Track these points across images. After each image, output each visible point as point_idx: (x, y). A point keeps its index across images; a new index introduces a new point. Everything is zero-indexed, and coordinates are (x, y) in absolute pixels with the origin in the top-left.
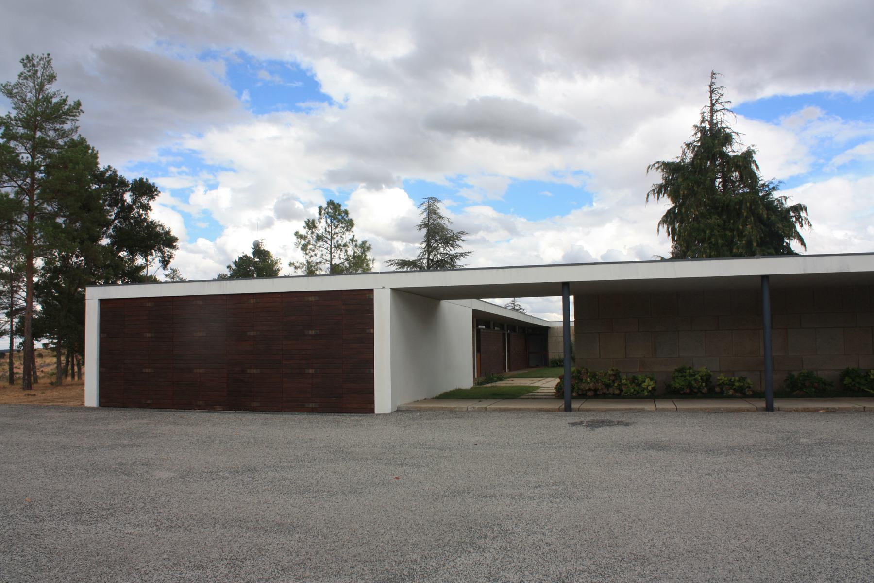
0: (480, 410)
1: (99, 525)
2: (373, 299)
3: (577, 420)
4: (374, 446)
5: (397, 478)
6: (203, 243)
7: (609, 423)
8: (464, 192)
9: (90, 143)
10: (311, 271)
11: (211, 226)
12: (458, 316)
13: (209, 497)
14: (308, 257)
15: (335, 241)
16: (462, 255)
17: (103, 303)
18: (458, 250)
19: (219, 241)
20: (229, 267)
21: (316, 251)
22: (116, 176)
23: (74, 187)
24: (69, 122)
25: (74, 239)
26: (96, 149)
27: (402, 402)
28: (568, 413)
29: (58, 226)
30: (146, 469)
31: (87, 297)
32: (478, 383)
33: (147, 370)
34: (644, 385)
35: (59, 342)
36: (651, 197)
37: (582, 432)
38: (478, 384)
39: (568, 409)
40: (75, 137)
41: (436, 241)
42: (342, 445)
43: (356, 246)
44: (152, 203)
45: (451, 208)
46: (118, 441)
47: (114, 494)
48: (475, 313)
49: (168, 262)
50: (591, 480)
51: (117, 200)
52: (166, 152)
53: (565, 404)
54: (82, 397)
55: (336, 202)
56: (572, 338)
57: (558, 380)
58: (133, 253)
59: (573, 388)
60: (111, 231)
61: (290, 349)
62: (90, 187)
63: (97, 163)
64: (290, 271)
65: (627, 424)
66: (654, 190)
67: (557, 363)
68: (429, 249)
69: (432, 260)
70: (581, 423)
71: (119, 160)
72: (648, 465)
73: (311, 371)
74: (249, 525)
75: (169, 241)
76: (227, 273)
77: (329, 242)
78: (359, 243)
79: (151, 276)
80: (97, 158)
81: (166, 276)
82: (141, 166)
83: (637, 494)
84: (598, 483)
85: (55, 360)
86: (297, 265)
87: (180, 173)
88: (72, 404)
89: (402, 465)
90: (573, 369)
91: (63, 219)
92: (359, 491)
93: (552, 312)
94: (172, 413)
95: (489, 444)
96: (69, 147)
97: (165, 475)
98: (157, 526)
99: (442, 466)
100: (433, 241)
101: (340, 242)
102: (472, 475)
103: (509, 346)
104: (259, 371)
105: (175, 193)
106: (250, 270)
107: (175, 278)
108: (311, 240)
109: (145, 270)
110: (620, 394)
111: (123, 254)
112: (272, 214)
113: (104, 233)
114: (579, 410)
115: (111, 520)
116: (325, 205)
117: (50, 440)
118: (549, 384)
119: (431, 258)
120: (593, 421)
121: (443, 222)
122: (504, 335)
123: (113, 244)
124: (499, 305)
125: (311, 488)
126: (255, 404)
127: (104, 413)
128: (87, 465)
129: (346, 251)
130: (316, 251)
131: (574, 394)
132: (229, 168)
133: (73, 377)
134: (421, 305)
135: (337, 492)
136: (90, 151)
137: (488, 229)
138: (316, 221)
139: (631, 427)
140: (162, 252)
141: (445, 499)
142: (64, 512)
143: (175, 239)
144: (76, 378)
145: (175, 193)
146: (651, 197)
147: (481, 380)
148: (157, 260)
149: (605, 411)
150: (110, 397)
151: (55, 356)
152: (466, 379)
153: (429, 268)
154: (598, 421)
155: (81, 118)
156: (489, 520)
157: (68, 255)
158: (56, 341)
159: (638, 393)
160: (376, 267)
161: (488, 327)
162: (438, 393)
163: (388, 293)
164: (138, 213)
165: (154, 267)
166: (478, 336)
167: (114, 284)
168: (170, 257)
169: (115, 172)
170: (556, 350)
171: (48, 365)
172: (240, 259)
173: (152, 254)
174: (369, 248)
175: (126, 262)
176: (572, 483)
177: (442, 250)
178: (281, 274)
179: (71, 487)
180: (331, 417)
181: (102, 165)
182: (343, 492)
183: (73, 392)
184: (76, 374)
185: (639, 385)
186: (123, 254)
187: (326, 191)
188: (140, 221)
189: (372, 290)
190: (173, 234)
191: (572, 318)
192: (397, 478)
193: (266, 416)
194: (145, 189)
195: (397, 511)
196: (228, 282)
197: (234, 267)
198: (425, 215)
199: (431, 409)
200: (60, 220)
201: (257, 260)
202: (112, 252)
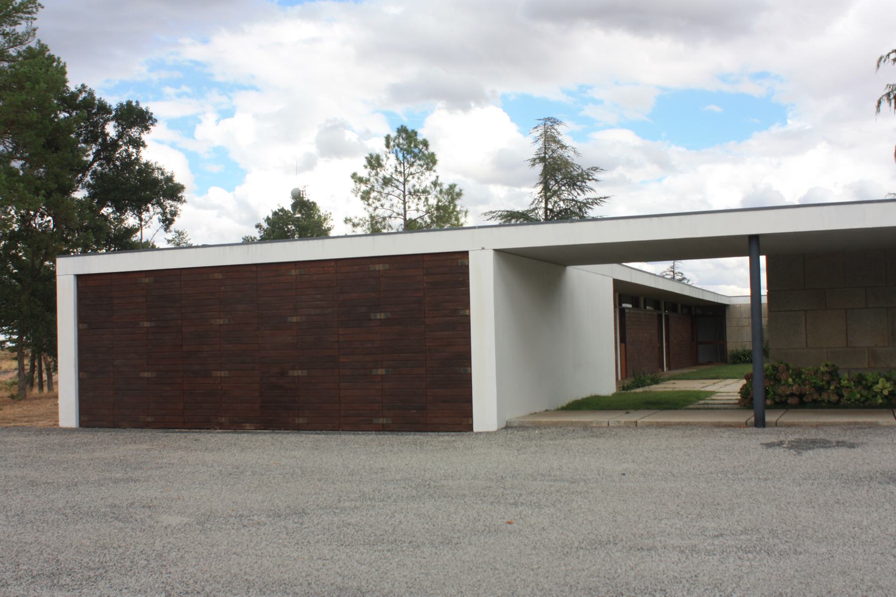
0: (627, 425)
1: (85, 591)
2: (467, 267)
3: (773, 439)
4: (475, 477)
5: (510, 523)
6: (216, 194)
7: (825, 444)
8: (589, 111)
9: (53, 51)
10: (376, 228)
11: (228, 170)
12: (592, 290)
13: (239, 550)
14: (371, 209)
15: (409, 186)
16: (595, 201)
17: (81, 279)
18: (590, 195)
19: (239, 190)
20: (258, 226)
21: (383, 201)
22: (94, 99)
23: (33, 116)
24: (23, 23)
25: (37, 192)
26: (62, 60)
27: (514, 415)
28: (760, 430)
29: (13, 173)
30: (148, 512)
31: (58, 273)
32: (623, 387)
33: (146, 375)
34: (877, 388)
35: (20, 338)
36: (885, 104)
37: (783, 457)
38: (624, 389)
39: (760, 423)
40: (33, 44)
41: (557, 182)
42: (428, 476)
43: (441, 191)
44: (145, 137)
45: (571, 134)
46: (108, 475)
47: (104, 547)
48: (617, 283)
49: (171, 221)
50: (799, 527)
51: (96, 135)
52: (157, 66)
53: (755, 416)
54: (54, 414)
55: (410, 128)
56: (765, 321)
57: (744, 382)
58: (120, 209)
59: (767, 392)
60: (88, 179)
61: (345, 343)
62: (56, 116)
63: (66, 81)
64: (348, 230)
65: (852, 446)
66: (888, 94)
67: (742, 358)
68: (547, 192)
69: (551, 210)
70: (780, 444)
71: (97, 75)
72: (887, 506)
73: (381, 372)
74: (297, 589)
75: (173, 191)
76: (256, 234)
77: (401, 187)
78: (445, 187)
79: (147, 243)
80: (65, 73)
81: (169, 241)
82: (124, 86)
83: (873, 549)
84: (810, 531)
85: (15, 364)
86: (356, 221)
87: (179, 96)
88: (41, 424)
89: (515, 504)
90: (766, 365)
91: (21, 162)
92: (455, 541)
93: (728, 284)
94: (183, 435)
95: (643, 475)
96: (25, 58)
97: (175, 520)
98: (166, 591)
99: (574, 505)
100: (553, 183)
101: (417, 187)
102: (619, 518)
103: (668, 335)
104: (305, 373)
105: (172, 124)
106: (289, 231)
107: (179, 244)
108: (376, 185)
109: (139, 234)
110: (839, 401)
111: (106, 211)
112: (313, 150)
113: (79, 182)
114: (776, 424)
115: (101, 584)
116: (394, 134)
117: (12, 473)
118: (730, 388)
119: (550, 206)
120: (799, 441)
121: (566, 154)
122: (660, 316)
123: (92, 197)
124: (650, 273)
125: (385, 537)
126: (301, 421)
127: (87, 436)
128: (65, 508)
129: (427, 199)
130: (383, 201)
131: (769, 402)
132: (249, 86)
133: (41, 387)
134: (538, 273)
135: (423, 544)
136: (55, 64)
137: (630, 164)
138: (383, 157)
139: (858, 450)
140: (164, 208)
141: (581, 552)
142: (35, 573)
143: (180, 188)
144: (46, 389)
145: (172, 124)
146: (885, 104)
147: (628, 382)
148: (156, 218)
149: (817, 426)
150: (93, 415)
151: (15, 359)
152: (605, 381)
153: (547, 220)
154: (806, 441)
155: (40, 15)
156: (648, 584)
157: (28, 214)
158: (15, 337)
159: (867, 399)
160: (468, 221)
161: (636, 305)
162: (565, 402)
163: (490, 256)
164: (126, 151)
165: (151, 229)
166: (622, 317)
167: (95, 252)
168: (174, 214)
169: (91, 94)
170: (740, 337)
171: (6, 372)
172: (275, 214)
173: (148, 210)
174: (459, 195)
175: (111, 223)
176: (771, 531)
177: (565, 195)
178: (332, 233)
179: (43, 538)
180: (410, 437)
181: (72, 85)
182: (432, 543)
183: (43, 408)
184: (45, 384)
185: (869, 388)
186: (106, 211)
187: (389, 115)
188: (129, 163)
189: (466, 253)
190: (177, 180)
191: (764, 291)
192: (510, 523)
193: (316, 436)
194: (135, 117)
195: (511, 569)
196: (259, 246)
197: (265, 225)
198: (540, 143)
199: (555, 425)
200: (16, 164)
201: (299, 215)
202: (90, 207)
